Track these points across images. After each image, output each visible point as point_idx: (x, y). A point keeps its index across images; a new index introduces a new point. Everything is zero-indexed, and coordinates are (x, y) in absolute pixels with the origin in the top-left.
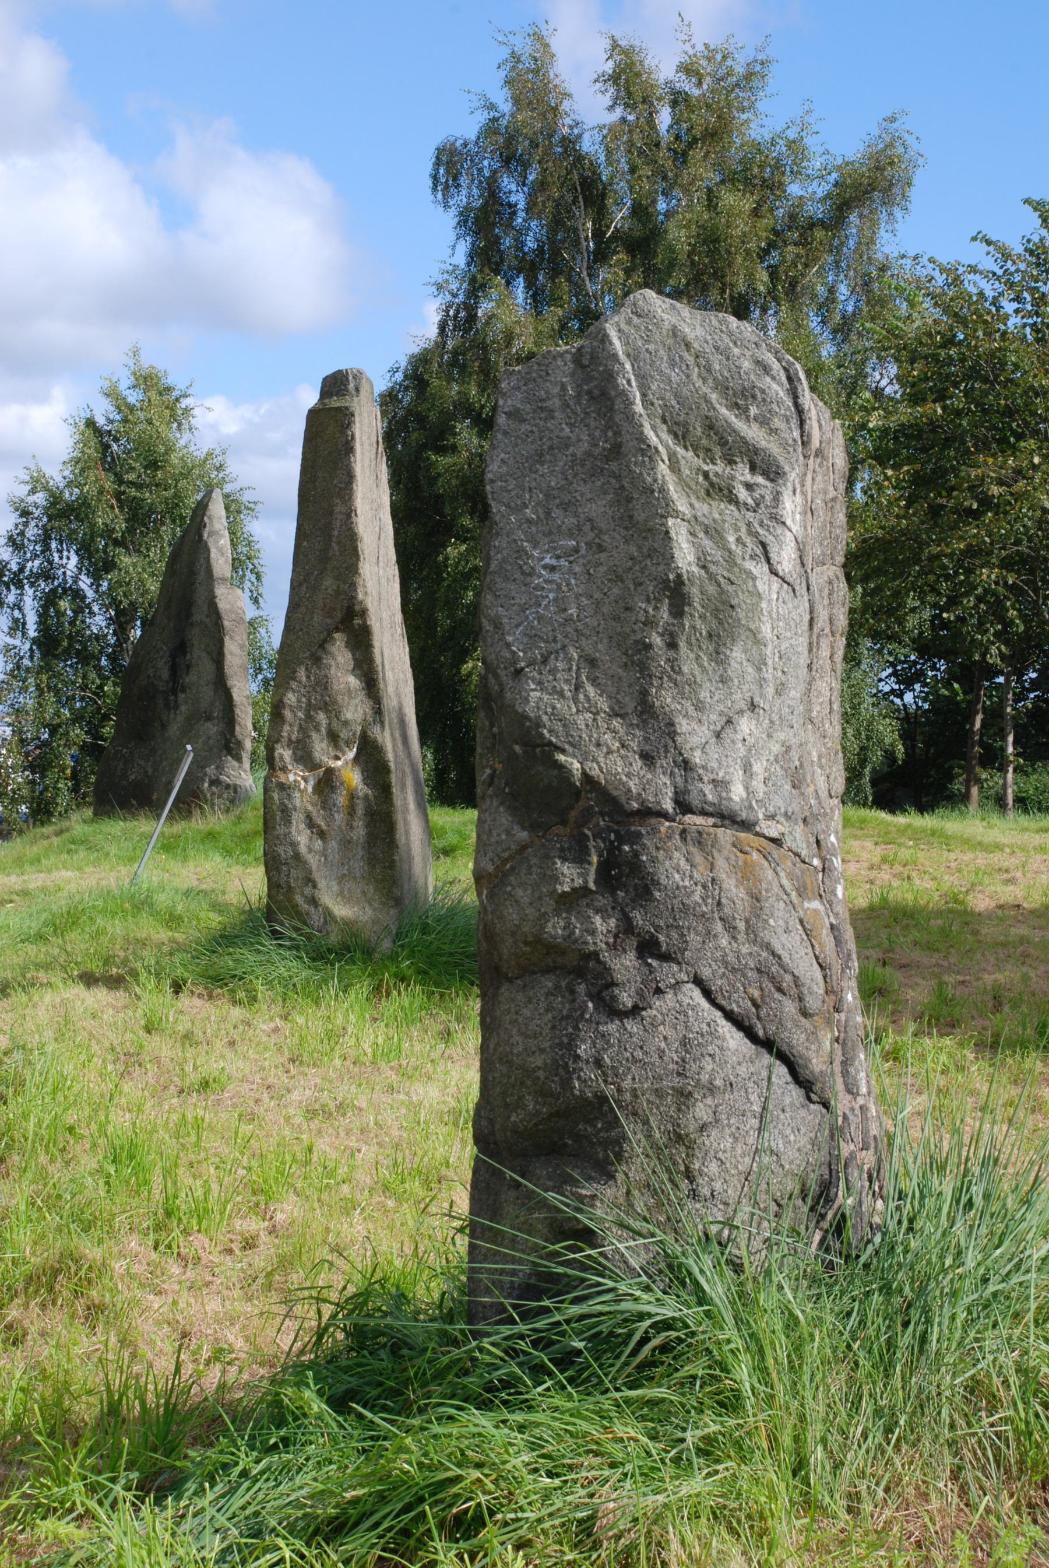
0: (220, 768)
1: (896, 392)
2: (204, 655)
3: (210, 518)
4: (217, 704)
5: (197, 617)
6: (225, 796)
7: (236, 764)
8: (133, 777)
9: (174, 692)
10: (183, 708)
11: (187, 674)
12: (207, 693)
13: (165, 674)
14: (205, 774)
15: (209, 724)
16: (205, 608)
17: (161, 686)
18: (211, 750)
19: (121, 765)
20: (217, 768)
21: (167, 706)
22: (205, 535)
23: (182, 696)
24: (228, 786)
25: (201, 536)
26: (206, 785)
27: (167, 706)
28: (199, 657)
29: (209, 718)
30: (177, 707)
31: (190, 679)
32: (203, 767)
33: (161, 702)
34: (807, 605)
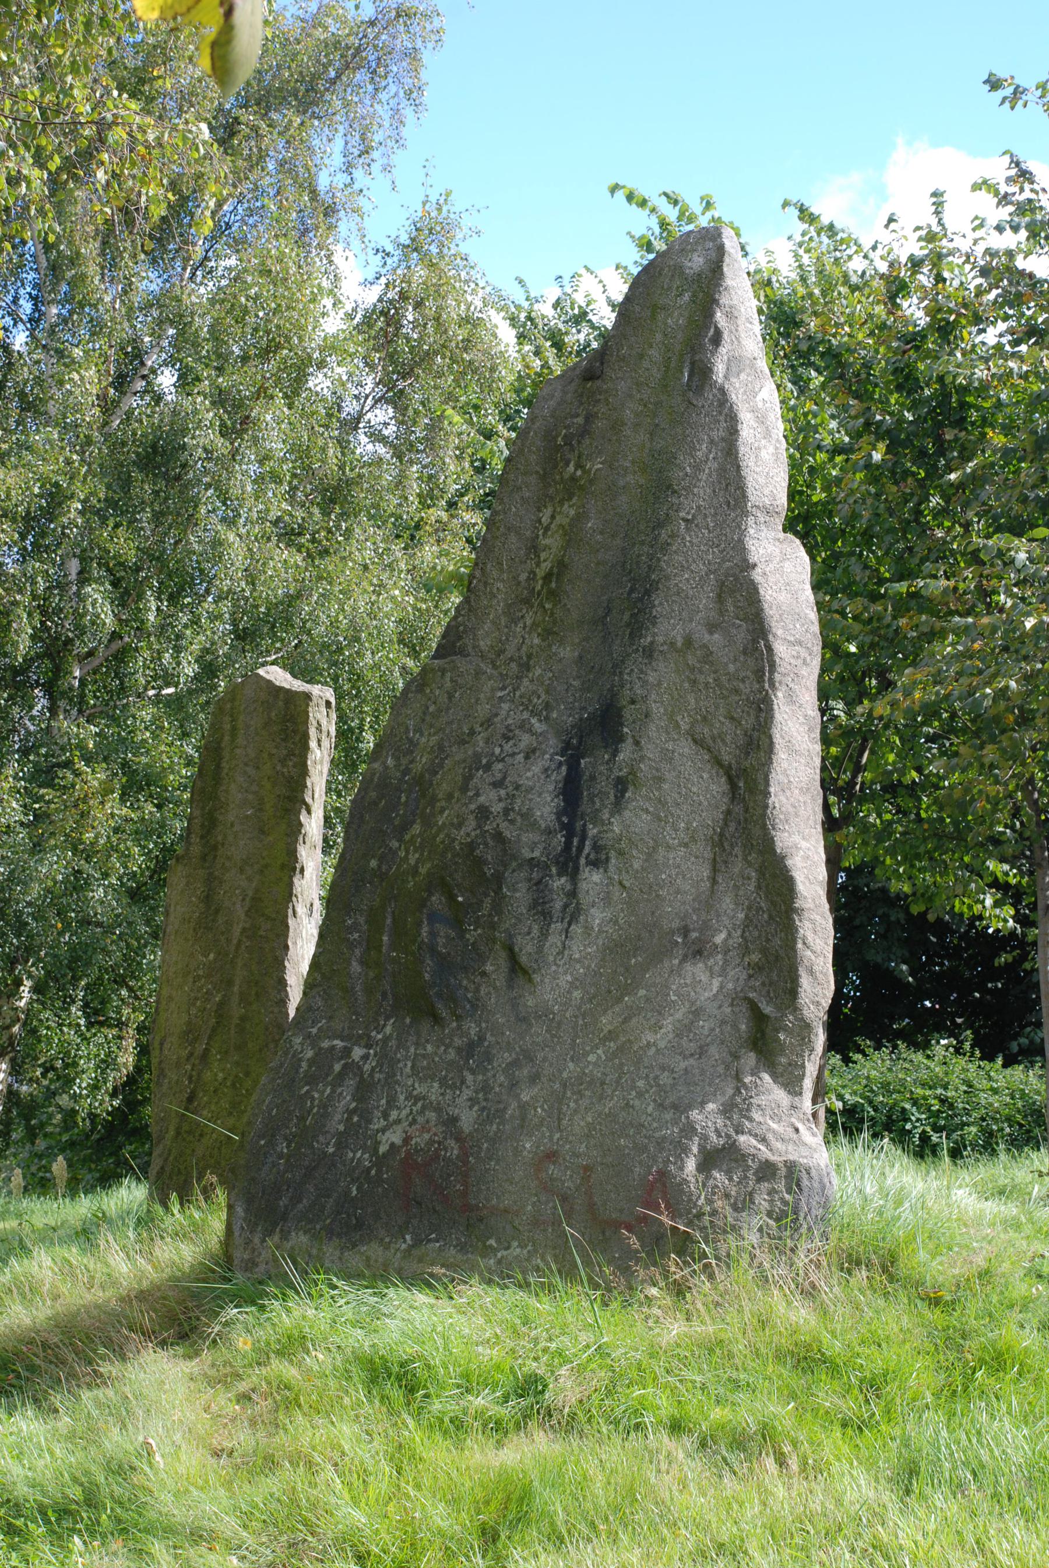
0: (737, 1109)
1: (386, 424)
2: (685, 747)
3: (730, 316)
4: (727, 903)
5: (669, 626)
6: (762, 1200)
7: (780, 1095)
8: (395, 1137)
9: (568, 863)
10: (597, 917)
11: (618, 805)
12: (682, 872)
13: (545, 806)
14: (690, 1130)
15: (697, 970)
16: (705, 601)
17: (531, 845)
18: (702, 1052)
19: (346, 1099)
20: (727, 1110)
21: (540, 908)
22: (720, 369)
23: (592, 879)
24: (767, 1171)
25: (702, 372)
26: (691, 1165)
27: (540, 908)
28: (667, 756)
29: (698, 951)
30: (573, 913)
31: (629, 823)
32: (681, 1108)
33: (519, 896)
34: (503, 954)
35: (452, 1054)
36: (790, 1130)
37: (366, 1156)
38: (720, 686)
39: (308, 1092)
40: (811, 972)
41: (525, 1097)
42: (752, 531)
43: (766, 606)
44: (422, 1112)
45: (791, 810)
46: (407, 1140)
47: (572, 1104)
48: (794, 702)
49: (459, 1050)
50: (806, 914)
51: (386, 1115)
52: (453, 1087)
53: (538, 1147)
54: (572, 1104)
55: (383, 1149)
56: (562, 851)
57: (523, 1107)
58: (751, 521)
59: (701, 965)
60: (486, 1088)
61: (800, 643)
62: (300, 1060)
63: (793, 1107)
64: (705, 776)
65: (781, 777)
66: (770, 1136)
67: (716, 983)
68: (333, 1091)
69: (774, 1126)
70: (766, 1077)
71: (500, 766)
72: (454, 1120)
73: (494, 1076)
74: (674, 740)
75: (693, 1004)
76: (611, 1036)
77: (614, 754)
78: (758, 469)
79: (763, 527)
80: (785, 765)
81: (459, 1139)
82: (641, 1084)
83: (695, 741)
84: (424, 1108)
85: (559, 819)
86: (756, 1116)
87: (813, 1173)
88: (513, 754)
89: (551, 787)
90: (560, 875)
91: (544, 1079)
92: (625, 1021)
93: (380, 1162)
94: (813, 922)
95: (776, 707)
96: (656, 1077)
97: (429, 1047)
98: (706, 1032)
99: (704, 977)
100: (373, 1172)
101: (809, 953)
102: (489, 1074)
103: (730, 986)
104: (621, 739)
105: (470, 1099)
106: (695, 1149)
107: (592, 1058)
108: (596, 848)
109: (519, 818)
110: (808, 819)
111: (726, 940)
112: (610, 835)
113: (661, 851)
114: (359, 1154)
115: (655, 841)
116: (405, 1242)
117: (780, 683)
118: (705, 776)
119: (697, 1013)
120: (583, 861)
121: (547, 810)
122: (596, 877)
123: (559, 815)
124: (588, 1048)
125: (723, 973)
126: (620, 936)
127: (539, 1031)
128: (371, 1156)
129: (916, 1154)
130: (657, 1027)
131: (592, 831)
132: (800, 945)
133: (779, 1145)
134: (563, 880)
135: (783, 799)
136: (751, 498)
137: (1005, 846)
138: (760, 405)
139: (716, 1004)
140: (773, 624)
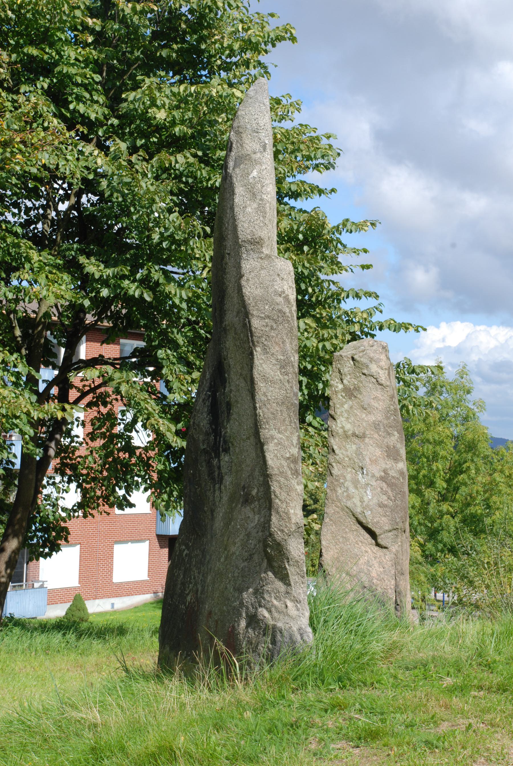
26: (243, 624)
36: (283, 606)
40: (278, 513)
42: (244, 256)
43: (246, 298)
45: (271, 416)
48: (267, 353)
50: (274, 478)
58: (243, 249)
59: (248, 508)
61: (268, 317)
63: (288, 593)
65: (263, 398)
66: (273, 609)
67: (257, 517)
69: (275, 602)
70: (270, 574)
75: (246, 529)
78: (244, 219)
79: (251, 252)
80: (264, 390)
86: (266, 596)
87: (285, 633)
89: (206, 410)
94: (279, 482)
95: (255, 357)
98: (252, 547)
99: (251, 515)
101: (277, 501)
103: (262, 520)
106: (244, 615)
110: (284, 420)
111: (257, 493)
117: (258, 342)
119: (248, 535)
121: (205, 422)
122: (227, 459)
123: (211, 424)
125: (259, 513)
132: (273, 496)
133: (276, 615)
135: (265, 410)
136: (240, 236)
138: (251, 181)
139: (255, 531)
140: (251, 308)
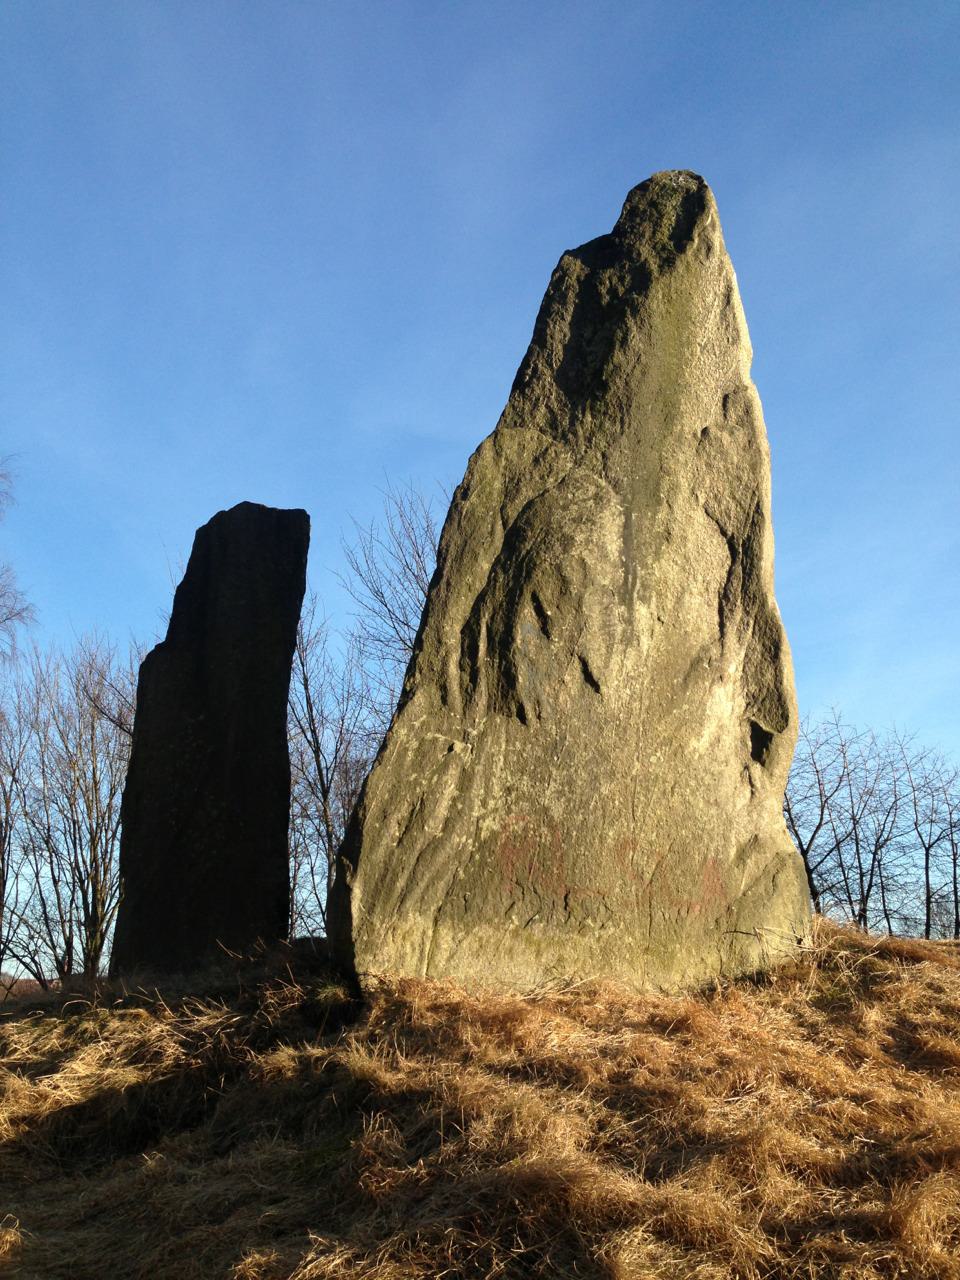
2: (699, 516)
31: (666, 568)
35: (539, 752)
37: (470, 841)
38: (727, 471)
39: (415, 779)
41: (605, 790)
44: (516, 803)
46: (504, 827)
47: (642, 798)
49: (545, 750)
51: (484, 804)
52: (542, 780)
53: (619, 836)
54: (642, 798)
55: (484, 835)
56: (623, 585)
57: (604, 801)
60: (570, 782)
62: (406, 749)
64: (715, 542)
68: (439, 779)
71: (576, 507)
72: (546, 810)
73: (576, 771)
74: (694, 510)
76: (669, 742)
77: (655, 514)
81: (552, 827)
82: (693, 783)
83: (706, 512)
84: (518, 798)
85: (620, 556)
88: (584, 501)
90: (620, 604)
91: (619, 776)
92: (678, 729)
93: (483, 846)
96: (702, 779)
97: (518, 744)
100: (477, 857)
102: (572, 770)
104: (659, 502)
105: (558, 792)
107: (653, 759)
108: (645, 587)
109: (596, 549)
112: (654, 578)
113: (687, 596)
114: (464, 839)
115: (683, 588)
116: (512, 922)
118: (715, 542)
120: (635, 595)
124: (649, 751)
126: (663, 660)
127: (610, 736)
128: (474, 842)
129: (454, 1009)
130: (699, 735)
131: (641, 572)
134: (623, 607)
137: (502, 744)
